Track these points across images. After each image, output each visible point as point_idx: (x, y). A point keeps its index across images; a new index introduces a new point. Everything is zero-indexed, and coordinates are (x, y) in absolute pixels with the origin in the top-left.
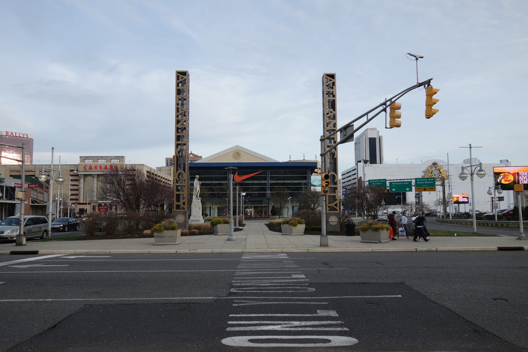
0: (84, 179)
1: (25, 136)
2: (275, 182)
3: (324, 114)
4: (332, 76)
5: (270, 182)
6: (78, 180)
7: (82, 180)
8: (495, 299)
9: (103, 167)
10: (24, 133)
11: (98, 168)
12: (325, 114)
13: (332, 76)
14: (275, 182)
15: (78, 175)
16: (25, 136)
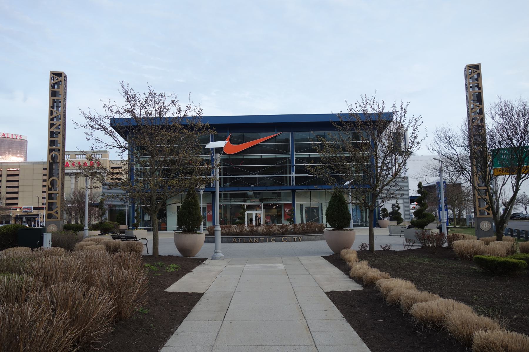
0: (76, 178)
1: (19, 138)
2: (305, 155)
3: (468, 109)
4: (477, 67)
5: (296, 155)
8: (435, 159)
10: (17, 134)
12: (470, 110)
13: (477, 67)
14: (305, 155)
16: (19, 138)
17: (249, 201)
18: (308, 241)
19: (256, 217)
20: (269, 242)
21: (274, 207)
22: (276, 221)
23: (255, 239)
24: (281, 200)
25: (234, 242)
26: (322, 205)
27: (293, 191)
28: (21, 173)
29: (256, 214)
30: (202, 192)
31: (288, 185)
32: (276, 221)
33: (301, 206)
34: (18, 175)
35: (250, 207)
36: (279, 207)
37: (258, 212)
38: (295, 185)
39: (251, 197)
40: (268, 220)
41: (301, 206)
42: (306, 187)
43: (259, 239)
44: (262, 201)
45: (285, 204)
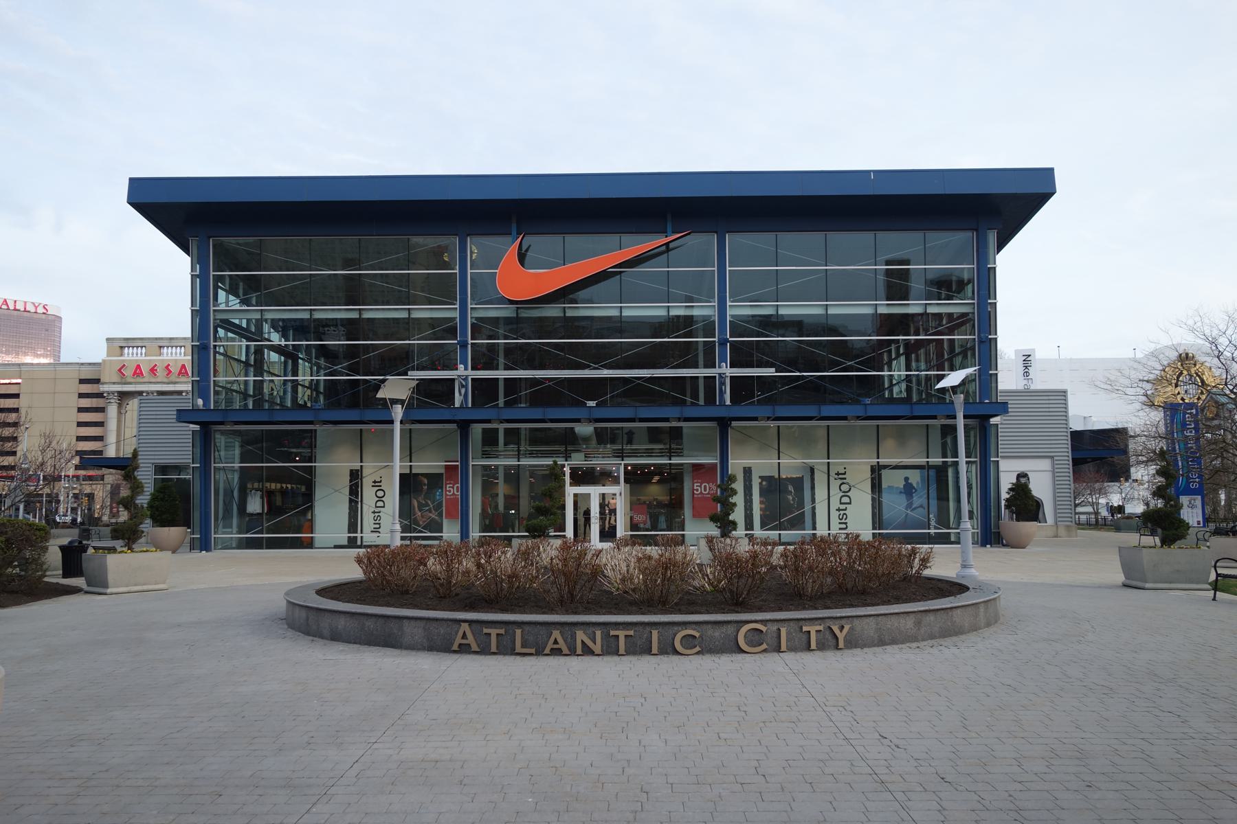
0: (120, 406)
1: (41, 310)
6: (102, 410)
7: (112, 410)
9: (175, 370)
10: (37, 301)
11: (161, 372)
15: (100, 395)
16: (41, 310)
17: (581, 455)
18: (881, 643)
19: (602, 506)
21: (656, 478)
22: (662, 519)
23: (581, 636)
24: (680, 454)
25: (464, 649)
26: (812, 470)
27: (724, 424)
28: (23, 391)
29: (603, 496)
30: (398, 412)
31: (702, 402)
32: (662, 519)
33: (748, 472)
34: (17, 396)
35: (582, 477)
36: (673, 478)
37: (609, 489)
38: (728, 403)
39: (586, 440)
40: (639, 518)
41: (748, 472)
42: (765, 410)
43: (606, 636)
44: (621, 455)
45: (694, 465)
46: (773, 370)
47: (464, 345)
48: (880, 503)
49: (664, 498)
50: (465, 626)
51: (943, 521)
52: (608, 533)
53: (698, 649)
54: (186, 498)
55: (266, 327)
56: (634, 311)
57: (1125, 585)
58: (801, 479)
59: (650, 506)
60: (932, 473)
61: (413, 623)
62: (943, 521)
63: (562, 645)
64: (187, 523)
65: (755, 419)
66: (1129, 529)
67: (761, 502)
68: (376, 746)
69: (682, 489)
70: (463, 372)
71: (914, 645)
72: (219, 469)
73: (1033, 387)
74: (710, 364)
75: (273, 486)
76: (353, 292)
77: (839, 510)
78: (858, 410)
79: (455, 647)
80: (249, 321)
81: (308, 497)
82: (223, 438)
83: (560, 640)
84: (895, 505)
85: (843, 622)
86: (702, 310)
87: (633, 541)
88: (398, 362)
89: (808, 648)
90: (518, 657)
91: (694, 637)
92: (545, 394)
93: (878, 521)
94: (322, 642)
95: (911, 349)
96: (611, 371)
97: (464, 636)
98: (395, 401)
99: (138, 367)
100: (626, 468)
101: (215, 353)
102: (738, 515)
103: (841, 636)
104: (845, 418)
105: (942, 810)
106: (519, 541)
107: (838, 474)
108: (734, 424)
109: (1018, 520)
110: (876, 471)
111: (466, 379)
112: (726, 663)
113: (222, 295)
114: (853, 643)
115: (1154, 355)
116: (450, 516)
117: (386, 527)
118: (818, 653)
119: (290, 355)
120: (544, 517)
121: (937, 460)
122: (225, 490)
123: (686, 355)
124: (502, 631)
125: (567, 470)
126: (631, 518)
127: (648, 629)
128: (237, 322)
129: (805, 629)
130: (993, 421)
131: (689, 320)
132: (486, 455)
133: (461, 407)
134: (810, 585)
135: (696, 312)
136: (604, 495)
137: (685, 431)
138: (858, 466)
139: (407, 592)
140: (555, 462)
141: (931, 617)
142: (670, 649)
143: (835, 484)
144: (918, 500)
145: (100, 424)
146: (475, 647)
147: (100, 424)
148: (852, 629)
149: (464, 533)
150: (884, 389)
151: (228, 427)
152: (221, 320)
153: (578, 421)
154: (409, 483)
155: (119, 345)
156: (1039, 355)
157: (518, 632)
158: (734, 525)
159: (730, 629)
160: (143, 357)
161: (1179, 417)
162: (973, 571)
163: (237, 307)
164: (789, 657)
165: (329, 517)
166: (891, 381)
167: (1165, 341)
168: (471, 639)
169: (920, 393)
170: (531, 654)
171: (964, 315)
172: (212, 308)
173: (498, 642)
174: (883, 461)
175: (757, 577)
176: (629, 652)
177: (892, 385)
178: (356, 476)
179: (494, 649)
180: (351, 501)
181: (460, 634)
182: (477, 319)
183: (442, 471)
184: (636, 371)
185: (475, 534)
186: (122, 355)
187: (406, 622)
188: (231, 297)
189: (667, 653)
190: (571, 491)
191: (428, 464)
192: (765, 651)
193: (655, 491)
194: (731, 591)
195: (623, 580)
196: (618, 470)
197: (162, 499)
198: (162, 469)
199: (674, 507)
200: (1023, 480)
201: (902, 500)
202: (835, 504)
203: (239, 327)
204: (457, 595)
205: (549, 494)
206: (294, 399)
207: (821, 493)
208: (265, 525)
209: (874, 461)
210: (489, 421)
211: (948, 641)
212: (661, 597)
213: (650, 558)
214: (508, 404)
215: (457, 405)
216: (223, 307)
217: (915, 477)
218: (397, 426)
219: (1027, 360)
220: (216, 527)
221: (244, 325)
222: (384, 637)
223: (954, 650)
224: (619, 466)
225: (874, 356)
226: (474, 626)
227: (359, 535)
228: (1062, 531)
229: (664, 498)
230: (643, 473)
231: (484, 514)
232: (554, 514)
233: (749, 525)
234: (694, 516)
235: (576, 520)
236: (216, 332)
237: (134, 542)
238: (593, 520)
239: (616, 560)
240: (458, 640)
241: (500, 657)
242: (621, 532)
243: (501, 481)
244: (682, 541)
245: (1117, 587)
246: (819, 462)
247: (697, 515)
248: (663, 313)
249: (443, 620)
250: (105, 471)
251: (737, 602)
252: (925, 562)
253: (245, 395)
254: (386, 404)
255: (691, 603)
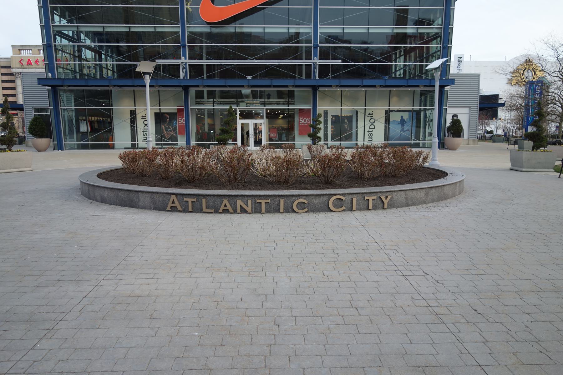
6: (13, 81)
15: (12, 74)
17: (244, 104)
18: (407, 205)
19: (255, 129)
20: (286, 211)
21: (281, 116)
22: (284, 136)
23: (239, 202)
25: (173, 209)
26: (357, 112)
27: (315, 88)
30: (147, 79)
31: (304, 77)
32: (284, 136)
33: (326, 113)
35: (246, 115)
36: (289, 116)
37: (258, 121)
38: (317, 78)
39: (247, 96)
40: (273, 135)
42: (336, 82)
43: (254, 203)
44: (264, 104)
45: (300, 110)
46: (340, 61)
47: (184, 46)
48: (389, 128)
49: (285, 126)
50: (174, 197)
51: (417, 137)
52: (258, 142)
53: (306, 210)
54: (48, 124)
55: (82, 36)
56: (271, 29)
57: (511, 169)
58: (351, 117)
59: (278, 129)
60: (415, 113)
61: (144, 194)
62: (417, 137)
63: (229, 207)
64: (49, 136)
65: (330, 86)
66: (499, 141)
67: (332, 128)
68: (103, 283)
69: (294, 121)
70: (184, 61)
71: (424, 206)
72: (64, 110)
73: (461, 73)
74: (309, 57)
75: (93, 118)
76: (128, 17)
77: (369, 132)
78: (381, 82)
79: (168, 208)
80: (73, 32)
81: (111, 124)
82: (65, 95)
83: (228, 205)
84: (395, 129)
85: (387, 194)
86: (305, 29)
87: (271, 146)
88: (151, 56)
89: (368, 208)
90: (204, 214)
91: (305, 203)
92: (228, 73)
93: (387, 136)
94: (95, 203)
95: (407, 53)
96: (259, 61)
97: (173, 202)
98: (145, 73)
99: (29, 60)
100: (266, 111)
101: (56, 49)
102: (321, 134)
103: (386, 202)
104: (374, 86)
105: (486, 342)
106: (213, 146)
107: (369, 114)
108: (320, 89)
109: (453, 137)
110: (388, 113)
111: (186, 64)
112: (322, 218)
113: (56, 18)
114: (392, 205)
115: (516, 58)
116: (181, 133)
117: (148, 139)
118: (373, 211)
119: (97, 52)
120: (226, 134)
121: (417, 108)
122: (68, 120)
123: (295, 53)
124: (195, 200)
125: (238, 113)
126: (269, 135)
127: (278, 199)
128: (66, 32)
129: (366, 198)
130: (446, 88)
131: (298, 34)
132: (197, 103)
133: (184, 79)
134: (367, 172)
135: (301, 31)
136: (256, 124)
137: (296, 93)
138: (379, 110)
139: (145, 176)
140: (231, 107)
141: (433, 191)
142: (290, 210)
143: (368, 119)
144: (407, 127)
145: (14, 88)
146: (179, 208)
147: (14, 88)
148: (392, 198)
149: (188, 142)
150: (392, 73)
151: (66, 88)
152: (57, 31)
153: (243, 86)
154: (159, 118)
155: (18, 49)
156: (466, 59)
157: (204, 200)
158: (320, 138)
159: (325, 199)
160: (31, 55)
161: (533, 88)
162: (437, 162)
163: (66, 24)
164: (357, 214)
165: (122, 136)
166: (396, 68)
167: (517, 54)
168: (177, 204)
169: (410, 75)
170: (212, 213)
171: (437, 34)
172: (51, 25)
173: (192, 205)
174: (391, 108)
175: (339, 169)
176: (267, 212)
177: (396, 71)
178: (133, 113)
179: (190, 209)
180: (131, 126)
181: (171, 201)
182: (190, 32)
183: (176, 111)
184: (272, 61)
185: (193, 143)
186: (20, 54)
187: (140, 194)
188: (62, 19)
189: (289, 212)
190: (240, 122)
191: (169, 108)
192: (344, 210)
193: (281, 122)
194: (324, 176)
195: (264, 170)
196: (263, 112)
197: (36, 125)
198: (37, 110)
199: (290, 129)
200: (455, 118)
201: (399, 127)
202: (367, 129)
203: (68, 36)
204: (172, 177)
205: (227, 123)
206: (101, 74)
207: (361, 124)
208: (89, 138)
209: (387, 108)
210: (198, 86)
211: (442, 203)
212: (285, 180)
213: (279, 158)
214: (208, 77)
215: (182, 77)
216: (57, 24)
217: (406, 116)
218: (148, 88)
219: (460, 60)
220: (65, 138)
221: (71, 35)
222: (129, 202)
223: (447, 209)
224: (263, 110)
225: (388, 55)
226: (178, 196)
227: (136, 143)
228: (471, 142)
229: (285, 126)
230: (275, 113)
231: (197, 132)
232: (231, 133)
233: (326, 139)
234: (299, 134)
235: (242, 136)
236: (55, 38)
237: (12, 146)
238: (250, 136)
239: (260, 156)
240: (170, 205)
241: (194, 214)
242: (264, 142)
243: (206, 117)
244: (293, 147)
245: (505, 170)
246: (360, 108)
247: (301, 133)
248: (285, 30)
249: (161, 193)
250: (18, 111)
251: (328, 183)
252: (425, 159)
253: (75, 72)
254: (140, 76)
255: (301, 183)
